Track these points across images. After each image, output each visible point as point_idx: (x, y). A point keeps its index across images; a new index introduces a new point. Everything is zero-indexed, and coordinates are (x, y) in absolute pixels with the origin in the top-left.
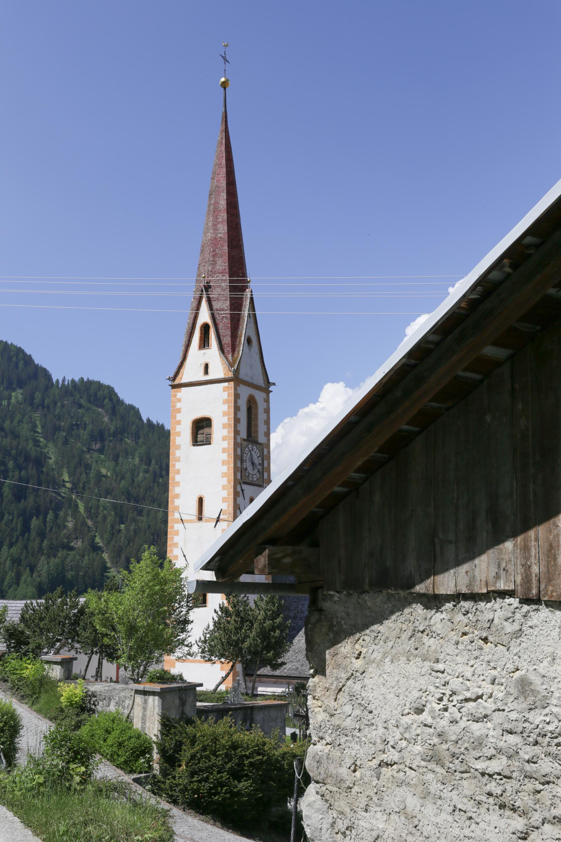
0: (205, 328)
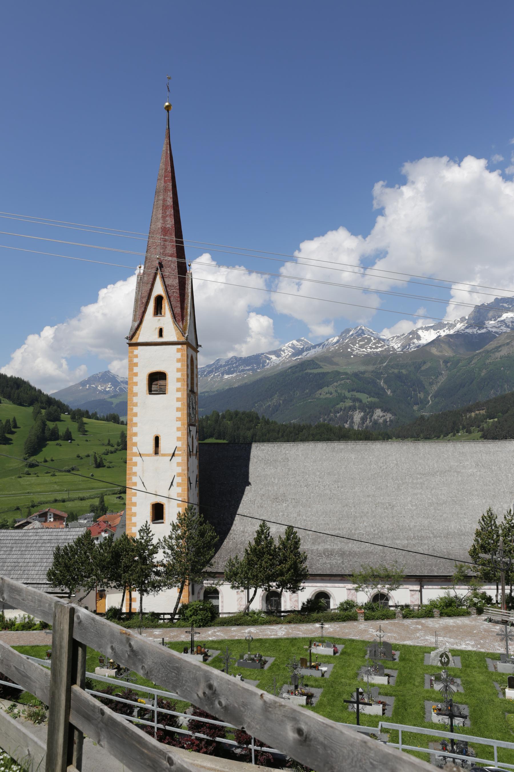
0: (159, 300)
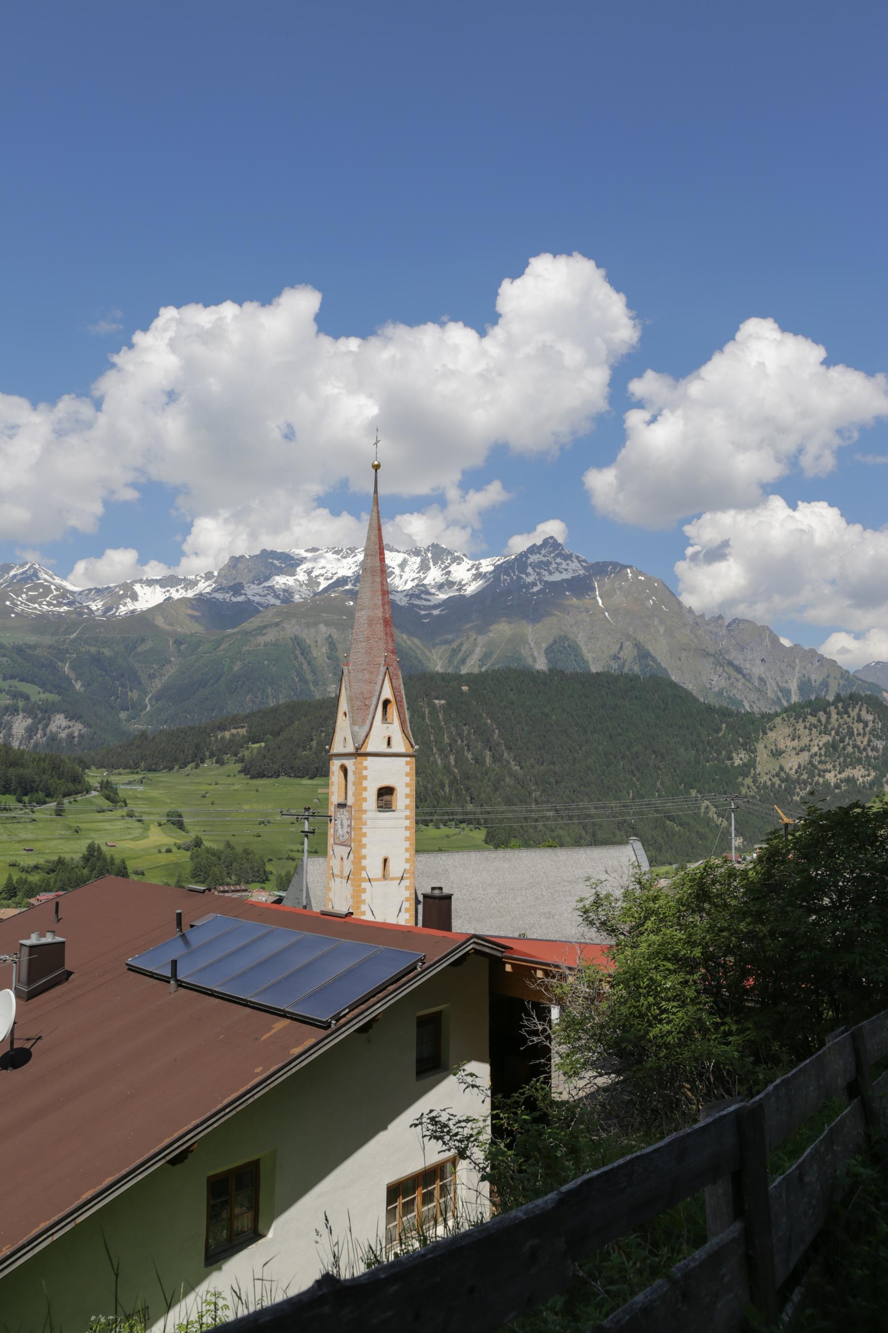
0: (386, 703)
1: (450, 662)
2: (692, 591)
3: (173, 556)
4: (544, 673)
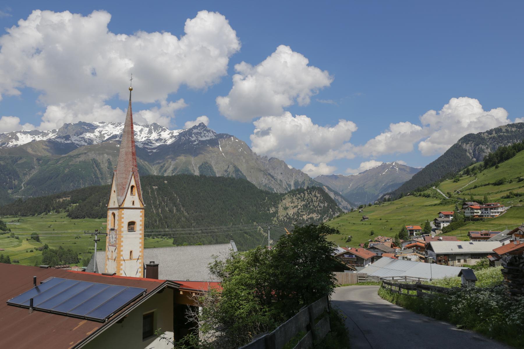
0: (132, 187)
1: (160, 171)
2: (256, 146)
3: (37, 122)
4: (198, 177)
